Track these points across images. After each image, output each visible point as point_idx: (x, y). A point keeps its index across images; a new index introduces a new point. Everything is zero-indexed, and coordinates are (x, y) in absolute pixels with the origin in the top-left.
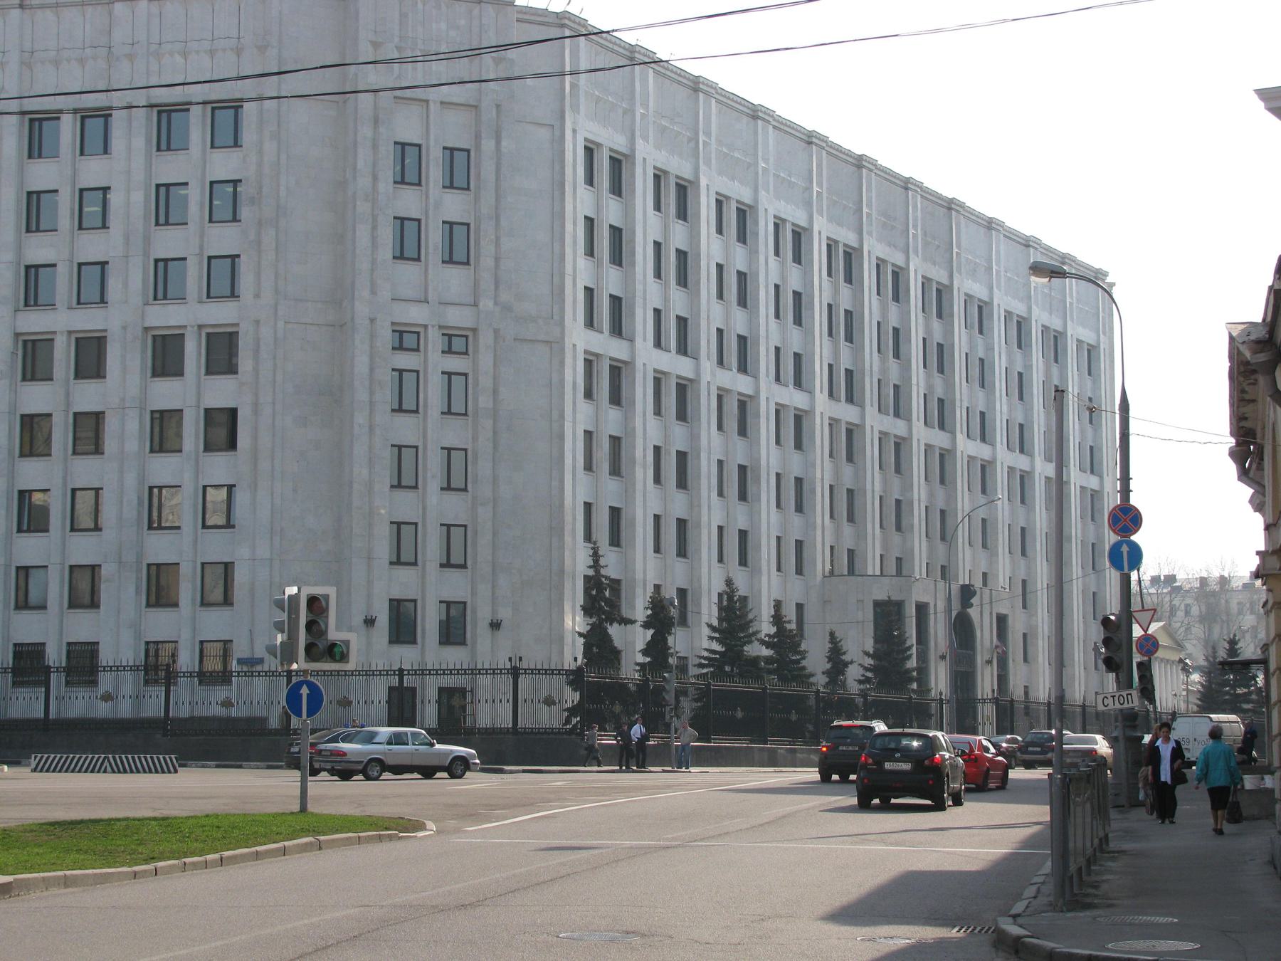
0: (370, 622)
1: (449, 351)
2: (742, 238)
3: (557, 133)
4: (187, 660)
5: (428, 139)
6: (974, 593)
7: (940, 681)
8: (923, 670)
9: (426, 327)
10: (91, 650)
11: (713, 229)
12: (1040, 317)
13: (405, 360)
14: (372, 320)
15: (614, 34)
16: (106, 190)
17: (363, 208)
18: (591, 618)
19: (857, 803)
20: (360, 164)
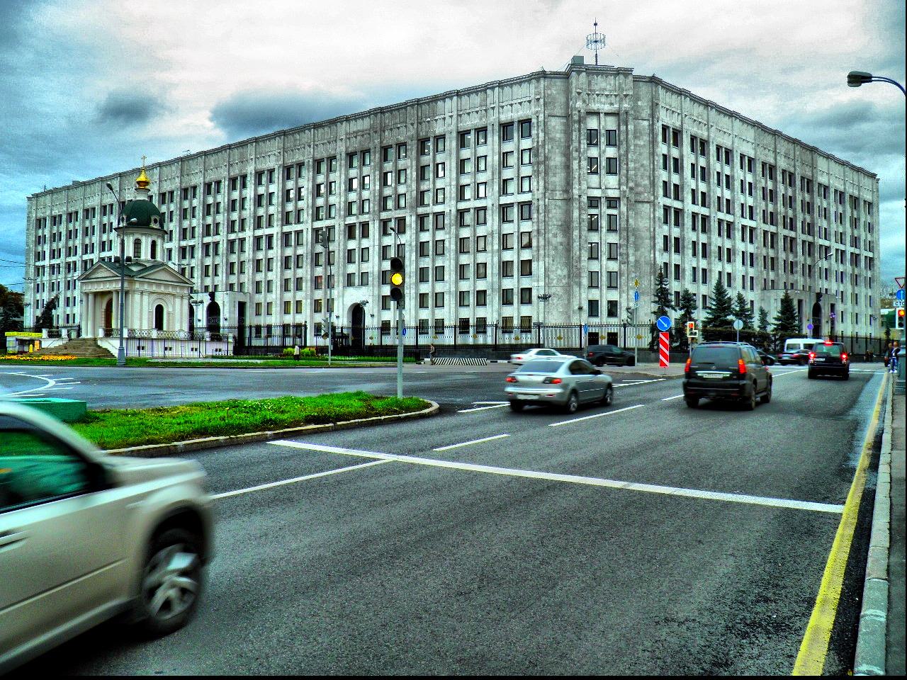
0: (580, 309)
1: (609, 207)
2: (727, 162)
3: (651, 122)
4: (516, 322)
5: (600, 127)
6: (821, 296)
10: (484, 319)
11: (715, 158)
12: (851, 190)
16: (486, 156)
17: (575, 154)
20: (574, 138)
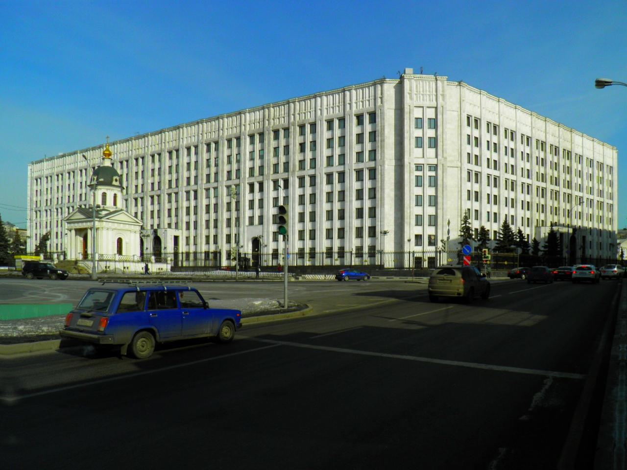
2: (512, 139)
7: (566, 255)
8: (562, 250)
9: (423, 164)
13: (420, 173)
14: (410, 163)
15: (111, 218)
18: (545, 247)
19: (316, 265)
